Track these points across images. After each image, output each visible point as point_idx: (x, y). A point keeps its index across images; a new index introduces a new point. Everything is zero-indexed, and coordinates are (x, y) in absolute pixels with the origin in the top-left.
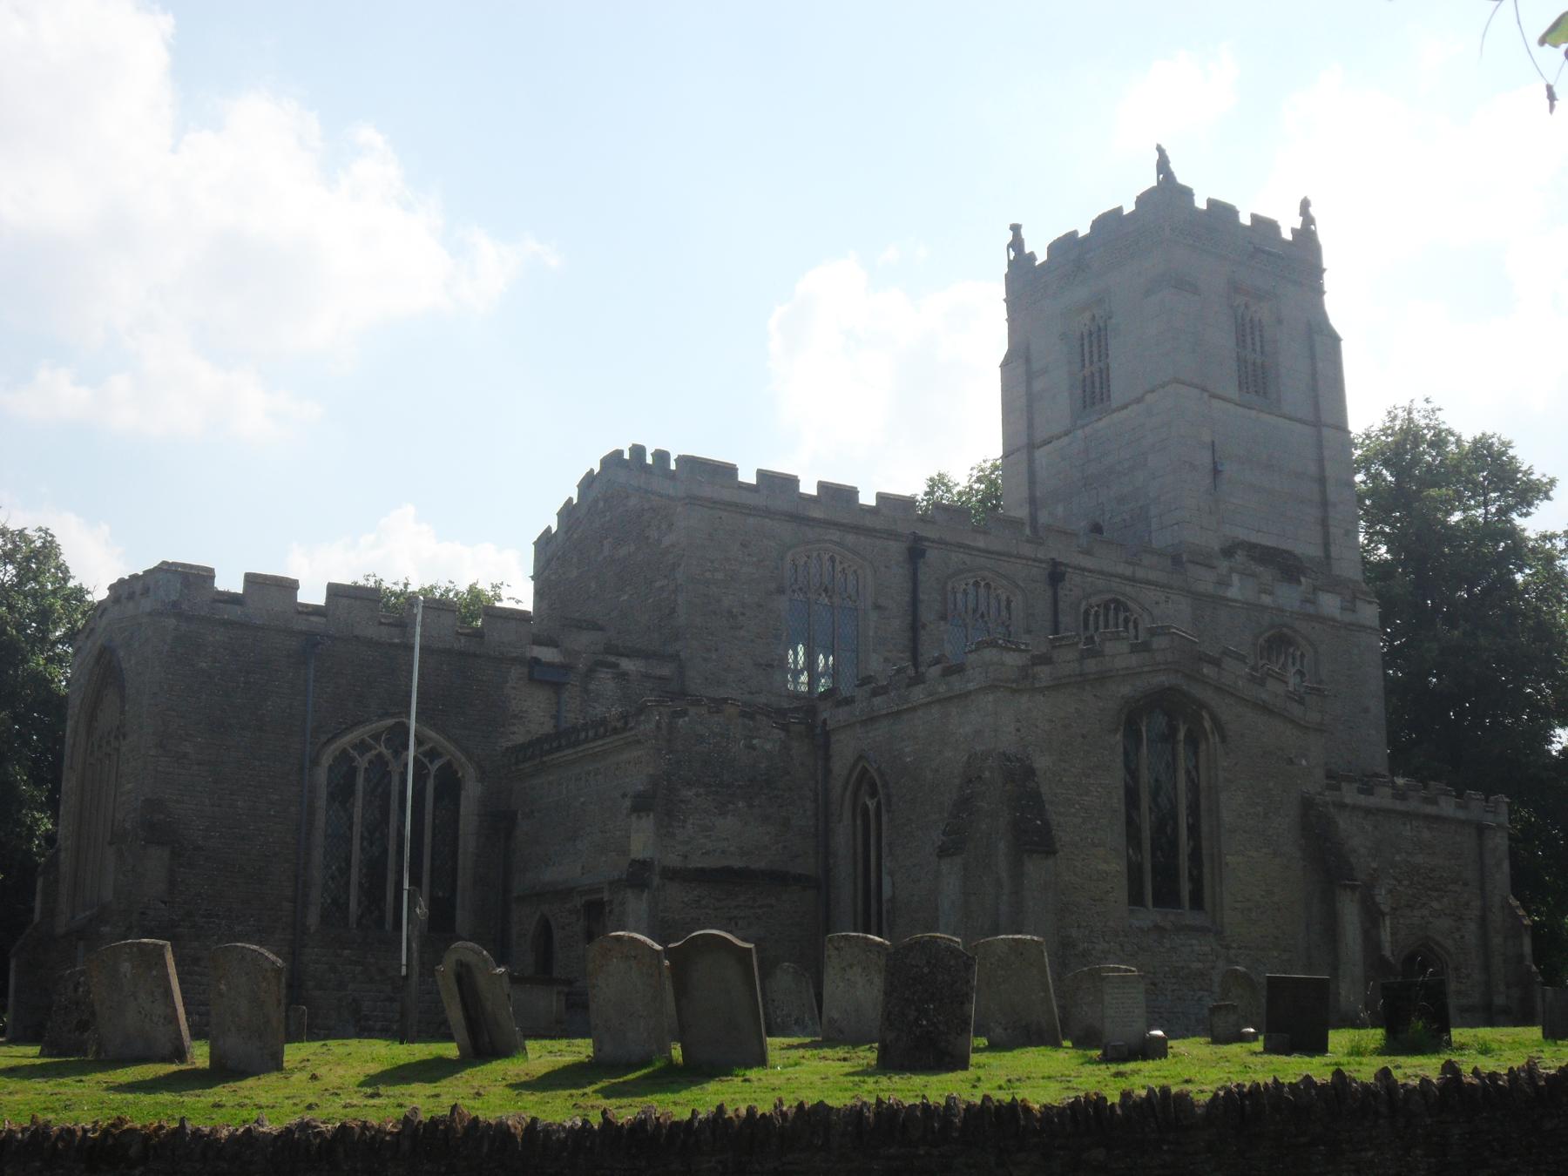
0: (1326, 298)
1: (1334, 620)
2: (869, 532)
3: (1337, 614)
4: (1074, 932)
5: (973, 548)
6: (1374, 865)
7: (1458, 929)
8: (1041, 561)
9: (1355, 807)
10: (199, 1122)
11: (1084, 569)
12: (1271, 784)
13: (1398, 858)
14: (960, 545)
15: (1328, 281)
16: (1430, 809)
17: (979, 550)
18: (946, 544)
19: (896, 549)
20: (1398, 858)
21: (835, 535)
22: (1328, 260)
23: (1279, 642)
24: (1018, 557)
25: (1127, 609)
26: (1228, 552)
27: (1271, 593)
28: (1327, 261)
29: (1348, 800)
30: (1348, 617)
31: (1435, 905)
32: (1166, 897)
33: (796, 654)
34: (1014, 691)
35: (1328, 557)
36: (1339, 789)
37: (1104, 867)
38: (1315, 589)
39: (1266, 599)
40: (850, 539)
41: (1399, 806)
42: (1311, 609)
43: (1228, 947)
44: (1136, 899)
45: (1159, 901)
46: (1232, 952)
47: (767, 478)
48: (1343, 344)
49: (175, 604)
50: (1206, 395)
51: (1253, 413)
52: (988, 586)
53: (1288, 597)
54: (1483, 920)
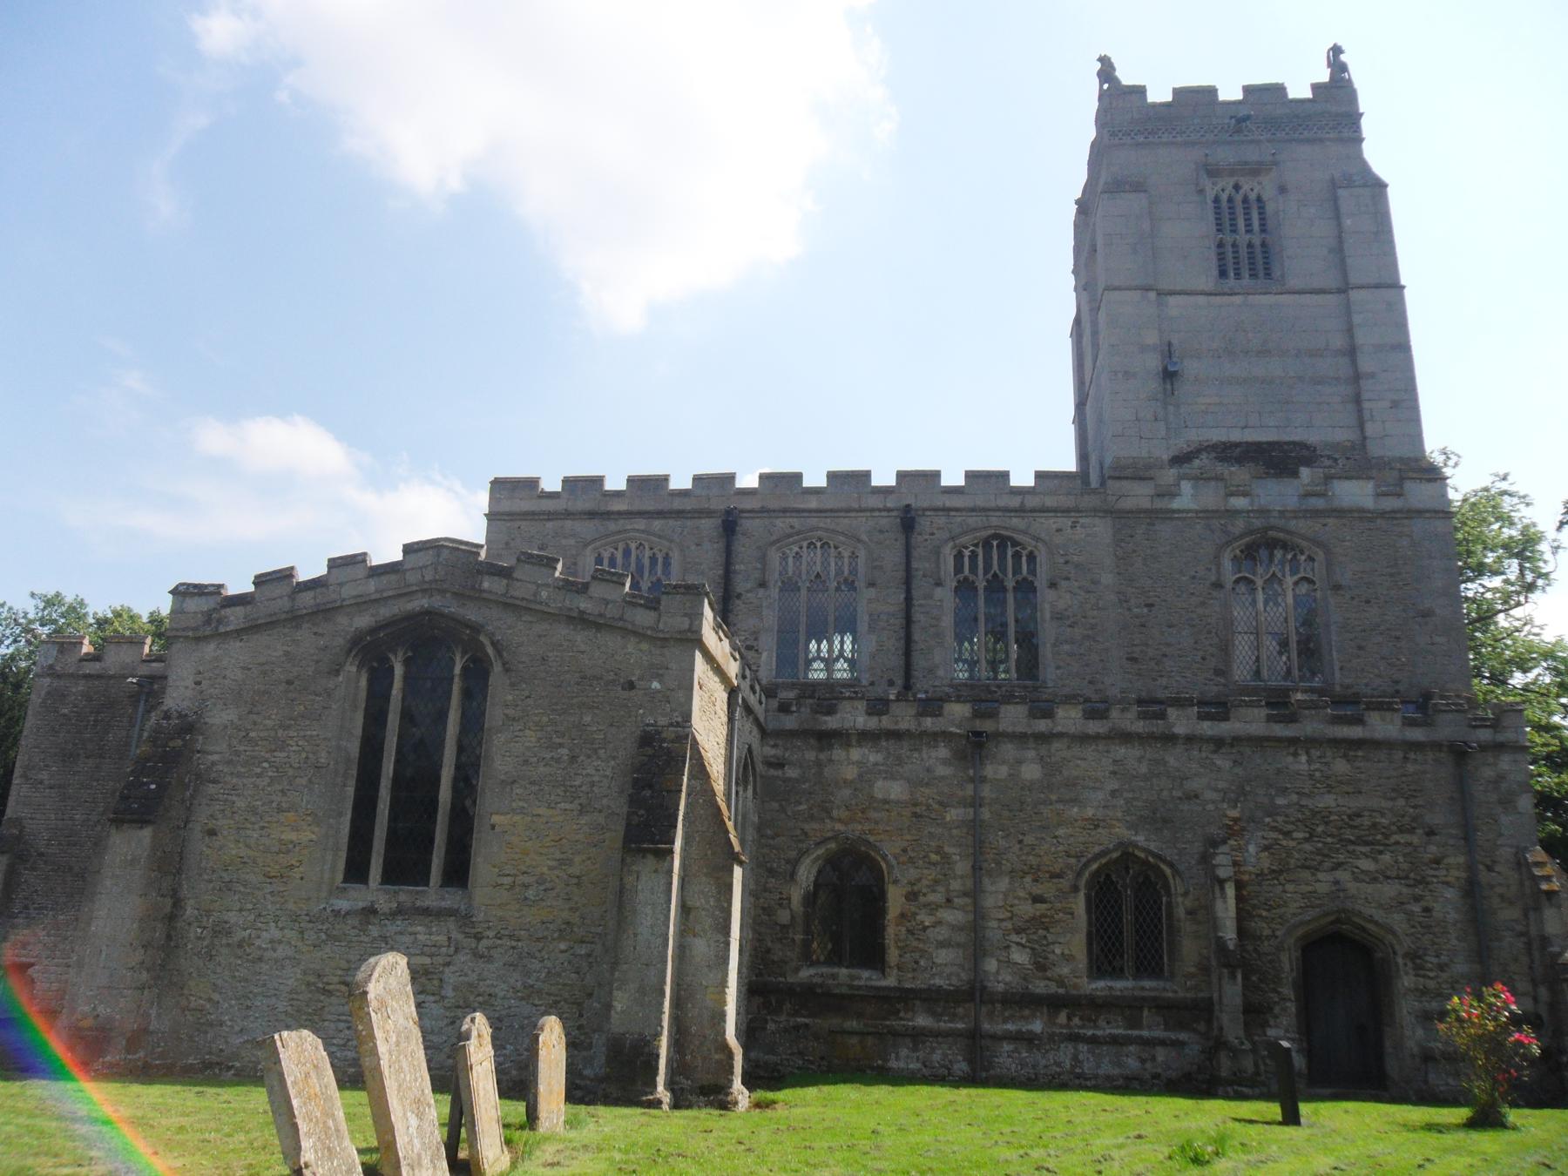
0: (1365, 145)
1: (1362, 510)
2: (679, 514)
3: (1369, 503)
4: (232, 917)
5: (804, 511)
6: (1234, 813)
7: (1417, 899)
8: (889, 510)
9: (1190, 739)
10: (472, 1045)
11: (950, 509)
12: (587, 719)
13: (1280, 801)
14: (785, 511)
15: (1365, 123)
16: (1355, 732)
17: (810, 511)
18: (768, 511)
19: (709, 526)
20: (1280, 801)
21: (641, 524)
22: (1366, 102)
23: (1263, 545)
24: (861, 510)
25: (1015, 543)
26: (1179, 460)
27: (1245, 494)
28: (1363, 106)
29: (1180, 730)
30: (1390, 503)
31: (1366, 865)
32: (406, 867)
33: (842, 643)
34: (198, 639)
35: (1365, 438)
36: (1162, 716)
37: (293, 836)
38: (1328, 478)
39: (1239, 503)
40: (657, 524)
41: (1094, 727)
42: (1319, 503)
43: (478, 937)
44: (356, 871)
45: (392, 875)
46: (484, 942)
47: (572, 484)
48: (1393, 195)
49: (51, 667)
50: (1152, 295)
51: (1237, 299)
52: (825, 545)
53: (1277, 495)
54: (1471, 890)
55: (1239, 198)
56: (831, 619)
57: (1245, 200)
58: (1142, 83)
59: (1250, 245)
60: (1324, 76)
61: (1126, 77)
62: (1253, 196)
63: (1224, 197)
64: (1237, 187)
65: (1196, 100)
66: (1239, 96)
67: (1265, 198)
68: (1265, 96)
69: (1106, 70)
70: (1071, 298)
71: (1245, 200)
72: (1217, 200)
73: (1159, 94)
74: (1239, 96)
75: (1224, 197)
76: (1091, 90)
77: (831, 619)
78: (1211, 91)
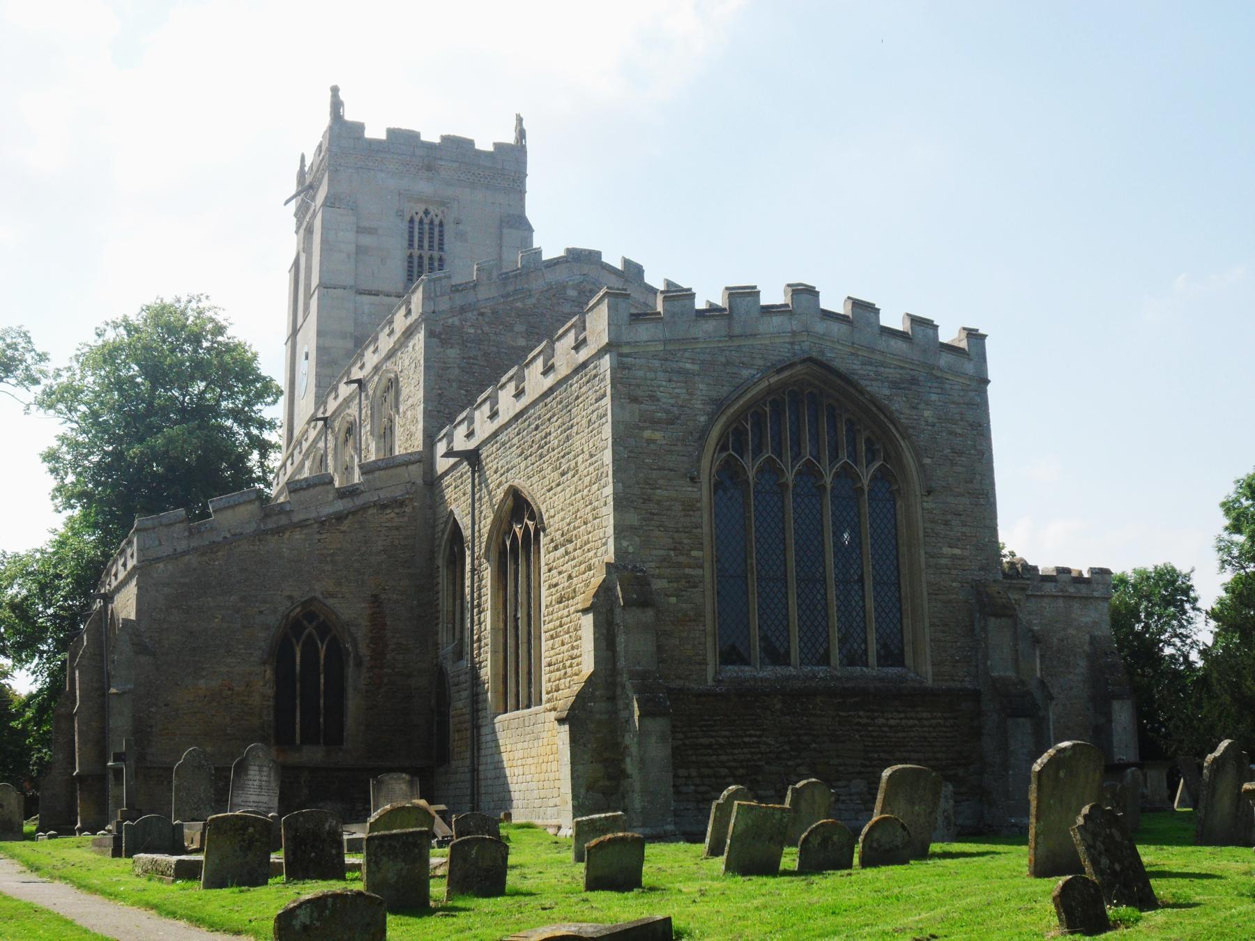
55: (426, 221)
56: (313, 889)
57: (432, 223)
58: (469, 137)
59: (420, 257)
60: (510, 138)
61: (349, 115)
62: (437, 222)
63: (417, 219)
64: (426, 212)
65: (403, 141)
66: (382, 136)
67: (445, 221)
68: (457, 148)
69: (336, 105)
70: (989, 393)
71: (432, 223)
72: (411, 221)
73: (375, 131)
74: (382, 136)
75: (417, 219)
76: (324, 120)
77: (313, 889)
78: (471, 142)
